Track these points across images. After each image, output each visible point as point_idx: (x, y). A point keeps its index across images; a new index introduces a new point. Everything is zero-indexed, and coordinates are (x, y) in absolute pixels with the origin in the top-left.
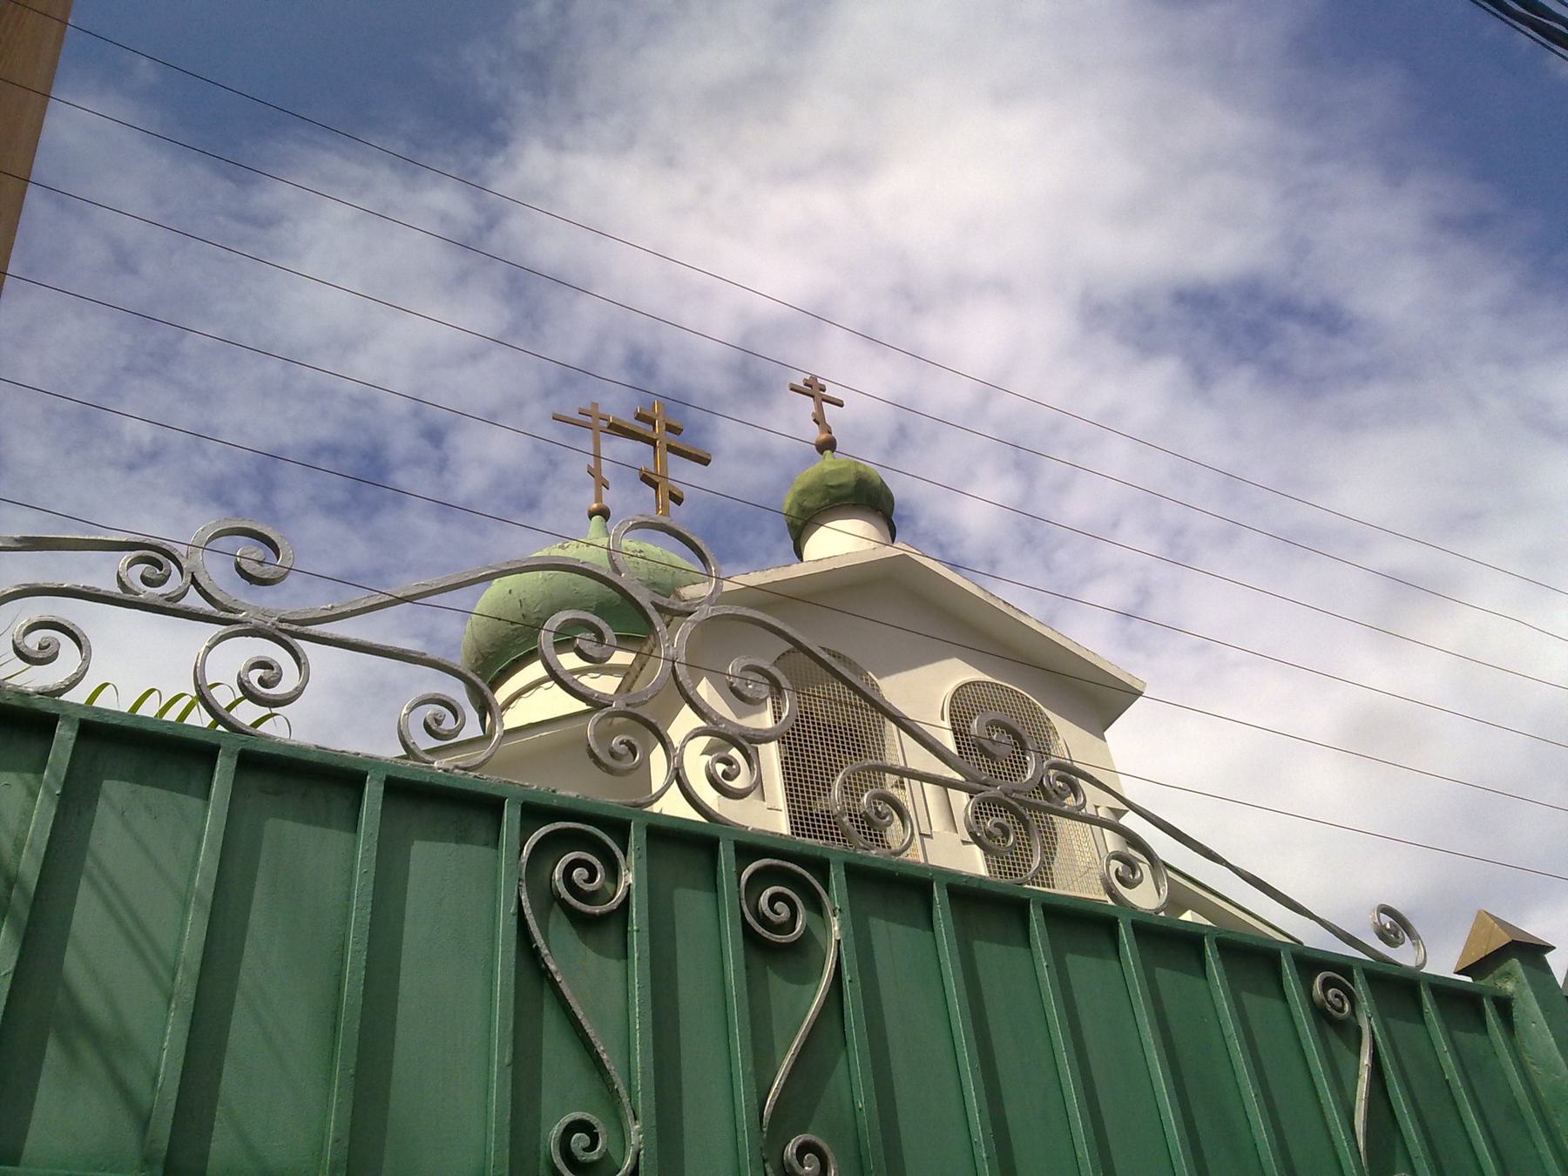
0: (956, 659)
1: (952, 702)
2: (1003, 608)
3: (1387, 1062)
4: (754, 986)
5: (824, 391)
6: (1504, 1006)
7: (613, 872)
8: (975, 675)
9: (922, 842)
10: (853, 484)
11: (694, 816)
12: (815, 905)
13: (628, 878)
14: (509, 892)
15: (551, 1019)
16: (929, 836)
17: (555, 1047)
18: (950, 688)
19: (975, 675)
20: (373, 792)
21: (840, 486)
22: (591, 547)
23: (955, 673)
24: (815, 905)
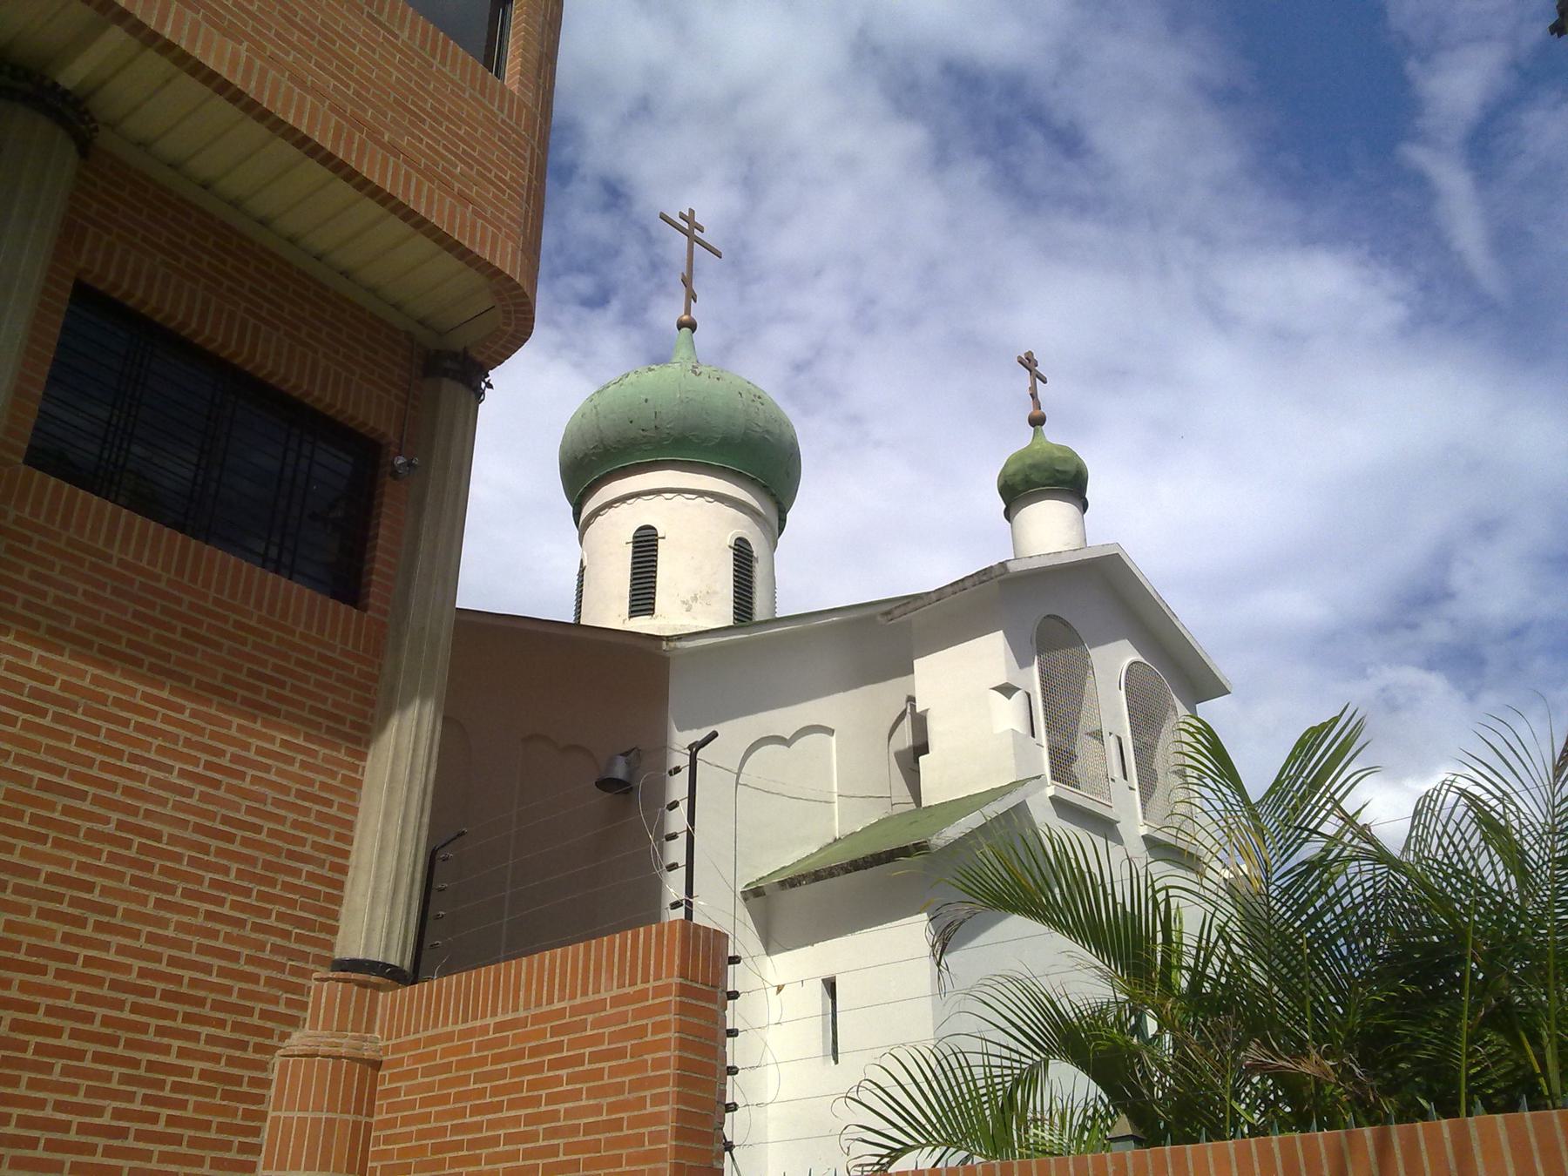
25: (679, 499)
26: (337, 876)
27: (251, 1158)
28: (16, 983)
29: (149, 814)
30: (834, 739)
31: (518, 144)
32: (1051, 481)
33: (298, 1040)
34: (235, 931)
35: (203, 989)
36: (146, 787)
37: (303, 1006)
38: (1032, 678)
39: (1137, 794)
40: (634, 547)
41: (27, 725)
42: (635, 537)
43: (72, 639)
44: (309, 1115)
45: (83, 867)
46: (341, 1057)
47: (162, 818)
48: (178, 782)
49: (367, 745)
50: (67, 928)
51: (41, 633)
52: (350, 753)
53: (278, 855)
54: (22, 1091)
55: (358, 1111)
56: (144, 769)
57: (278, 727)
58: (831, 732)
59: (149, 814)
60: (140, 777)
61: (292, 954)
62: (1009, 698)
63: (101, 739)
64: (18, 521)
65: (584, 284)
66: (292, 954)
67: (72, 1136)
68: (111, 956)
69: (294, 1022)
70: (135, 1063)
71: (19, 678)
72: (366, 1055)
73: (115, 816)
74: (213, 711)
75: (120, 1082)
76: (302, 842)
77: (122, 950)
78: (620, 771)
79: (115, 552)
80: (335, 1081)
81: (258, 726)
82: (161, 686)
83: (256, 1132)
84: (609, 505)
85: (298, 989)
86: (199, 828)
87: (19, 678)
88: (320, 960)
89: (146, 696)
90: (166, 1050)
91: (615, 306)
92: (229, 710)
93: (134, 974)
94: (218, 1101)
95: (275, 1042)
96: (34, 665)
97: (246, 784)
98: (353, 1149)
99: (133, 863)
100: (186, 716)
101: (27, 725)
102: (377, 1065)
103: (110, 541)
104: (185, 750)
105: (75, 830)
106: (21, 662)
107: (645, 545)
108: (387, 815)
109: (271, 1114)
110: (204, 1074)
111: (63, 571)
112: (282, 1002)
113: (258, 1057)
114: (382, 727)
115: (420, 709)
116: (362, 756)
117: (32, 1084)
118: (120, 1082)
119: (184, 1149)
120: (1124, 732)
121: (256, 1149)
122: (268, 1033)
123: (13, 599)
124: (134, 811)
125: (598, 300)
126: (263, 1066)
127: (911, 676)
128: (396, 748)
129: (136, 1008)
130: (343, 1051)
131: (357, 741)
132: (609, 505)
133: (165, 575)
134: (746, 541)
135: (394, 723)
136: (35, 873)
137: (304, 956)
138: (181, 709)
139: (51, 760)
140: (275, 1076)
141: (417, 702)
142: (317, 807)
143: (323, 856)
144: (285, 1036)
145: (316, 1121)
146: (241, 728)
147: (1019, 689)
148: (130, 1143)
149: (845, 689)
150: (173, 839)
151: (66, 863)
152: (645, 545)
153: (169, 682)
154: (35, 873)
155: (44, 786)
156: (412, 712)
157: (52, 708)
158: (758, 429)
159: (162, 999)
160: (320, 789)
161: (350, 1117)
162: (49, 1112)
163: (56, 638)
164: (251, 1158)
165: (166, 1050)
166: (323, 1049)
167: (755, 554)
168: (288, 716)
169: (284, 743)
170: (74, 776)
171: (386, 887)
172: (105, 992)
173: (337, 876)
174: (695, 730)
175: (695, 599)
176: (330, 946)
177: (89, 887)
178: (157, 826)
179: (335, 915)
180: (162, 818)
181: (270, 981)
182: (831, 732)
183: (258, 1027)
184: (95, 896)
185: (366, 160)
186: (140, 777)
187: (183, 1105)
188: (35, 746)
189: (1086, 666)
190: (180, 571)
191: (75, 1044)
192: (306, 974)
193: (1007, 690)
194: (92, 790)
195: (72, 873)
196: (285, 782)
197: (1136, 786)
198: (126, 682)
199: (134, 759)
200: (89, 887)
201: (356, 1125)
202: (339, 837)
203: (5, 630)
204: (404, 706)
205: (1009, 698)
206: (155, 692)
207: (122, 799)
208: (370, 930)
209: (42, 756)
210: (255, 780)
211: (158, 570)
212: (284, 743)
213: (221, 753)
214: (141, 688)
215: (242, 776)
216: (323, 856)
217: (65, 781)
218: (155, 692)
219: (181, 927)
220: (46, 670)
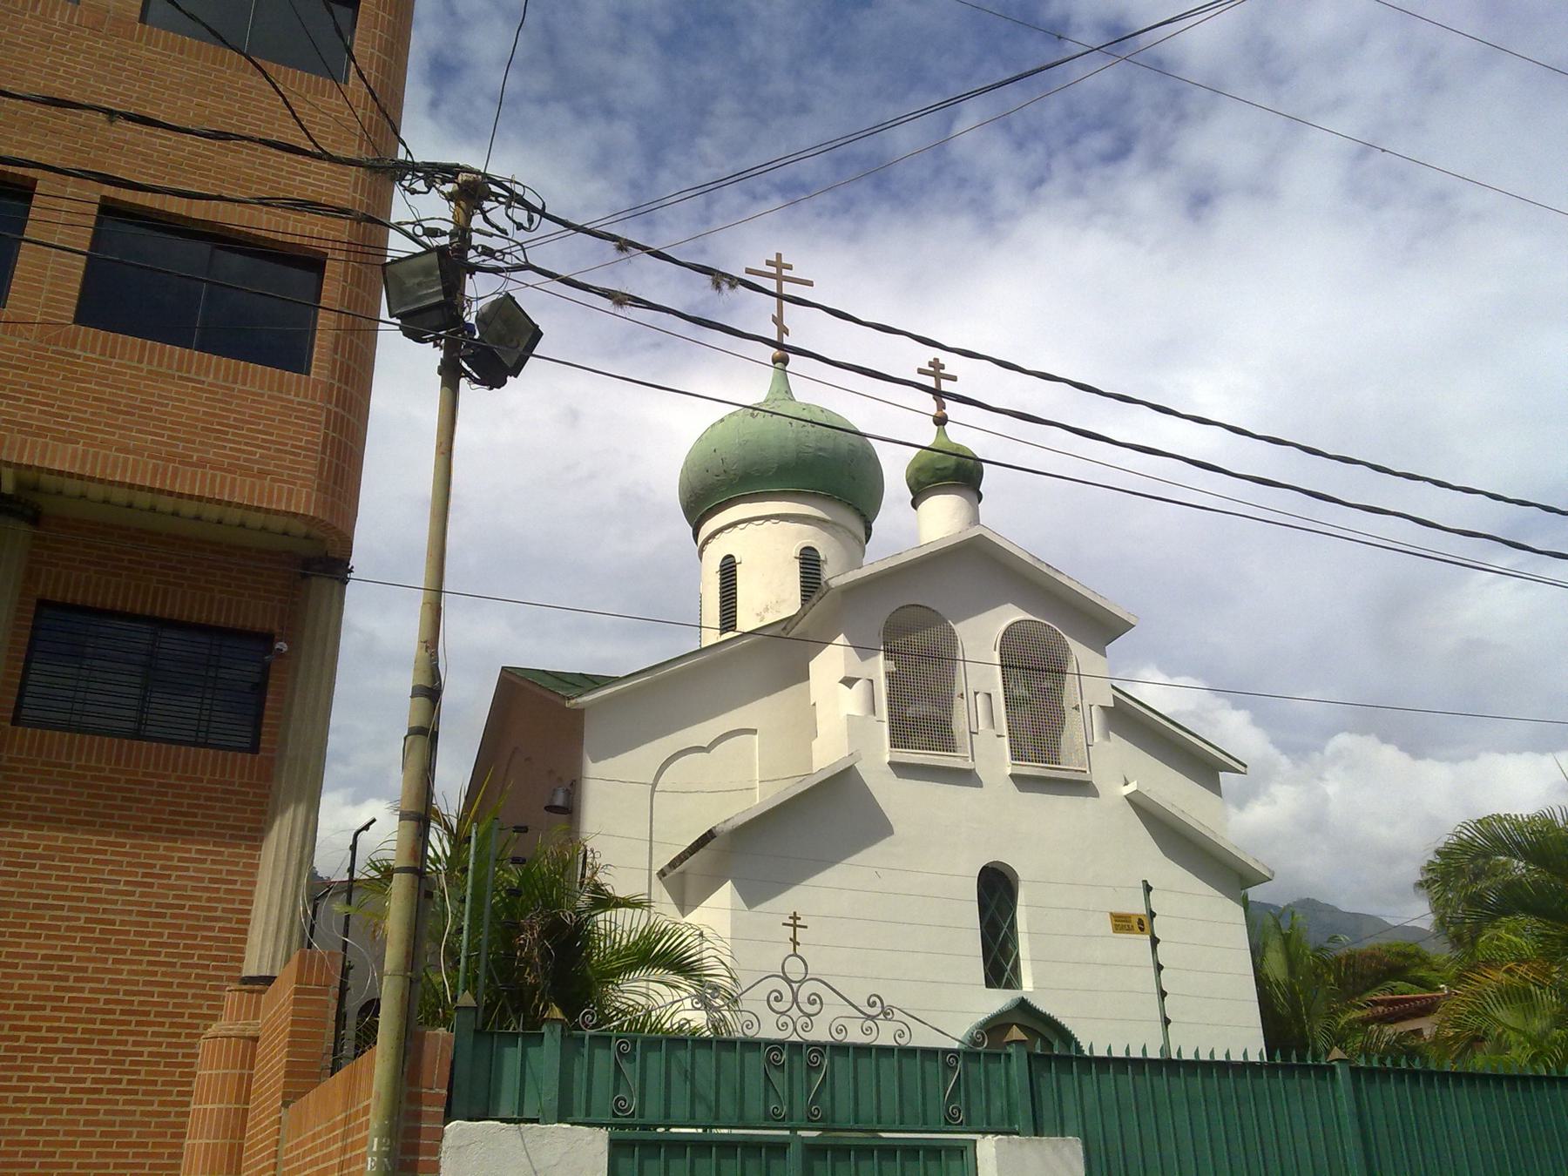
0: (1010, 605)
1: (1002, 640)
2: (1045, 569)
3: (962, 1077)
4: (808, 1075)
5: (943, 368)
6: (1009, 1056)
7: (782, 1055)
8: (1021, 615)
9: (971, 738)
10: (953, 467)
11: (800, 1040)
12: (822, 1056)
13: (784, 1056)
14: (763, 1064)
15: (771, 1088)
16: (977, 733)
17: (772, 1093)
18: (1003, 627)
19: (1021, 615)
20: (738, 1045)
21: (945, 468)
22: (775, 416)
23: (1011, 615)
24: (822, 1056)
25: (751, 526)
26: (242, 926)
27: (186, 1099)
28: (27, 1017)
29: (105, 911)
30: (757, 736)
31: (313, 414)
32: (933, 480)
33: (215, 1028)
34: (170, 970)
35: (148, 1006)
36: (103, 896)
37: (221, 1008)
38: (879, 666)
39: (1006, 740)
40: (721, 575)
41: (24, 875)
42: (721, 566)
43: (48, 819)
44: (214, 1072)
45: (64, 948)
46: (231, 1037)
47: (114, 912)
48: (125, 888)
49: (262, 841)
50: (56, 983)
51: (29, 821)
52: (249, 847)
53: (198, 920)
54: (35, 1073)
55: (242, 1067)
56: (101, 885)
57: (193, 842)
58: (754, 732)
59: (105, 911)
60: (99, 890)
61: (210, 978)
62: (850, 688)
63: (72, 874)
64: (10, 760)
65: (1099, 142)
66: (210, 978)
67: (67, 1095)
68: (86, 995)
69: (214, 1018)
70: (105, 1052)
71: (16, 850)
72: (247, 1034)
73: (83, 916)
74: (146, 842)
75: (95, 1063)
76: (215, 909)
77: (92, 990)
78: (559, 800)
79: (73, 761)
80: (228, 1051)
81: (179, 844)
82: (109, 834)
83: (190, 1084)
84: (721, 530)
85: (217, 998)
86: (140, 913)
87: (16, 850)
88: (231, 979)
89: (99, 843)
90: (125, 1043)
91: (1141, 150)
92: (157, 839)
93: (101, 1003)
94: (161, 1068)
95: (200, 1031)
96: (25, 840)
97: (172, 881)
98: (239, 1090)
99: (97, 940)
100: (127, 849)
101: (24, 875)
102: (255, 1039)
103: (69, 756)
104: (128, 869)
105: (58, 928)
106: (17, 840)
107: (728, 570)
108: (273, 882)
109: (199, 1073)
110: (151, 1054)
111: (40, 782)
112: (205, 1007)
113: (188, 1041)
114: (271, 827)
115: (294, 811)
116: (259, 848)
117: (41, 1069)
118: (95, 1063)
119: (140, 1097)
120: (996, 687)
121: (190, 1094)
122: (197, 1026)
123: (9, 806)
124: (96, 911)
125: (1119, 153)
126: (192, 1046)
127: (806, 683)
128: (278, 840)
129: (103, 1022)
130: (231, 1033)
131: (255, 839)
132: (721, 530)
133: (108, 768)
134: (813, 549)
135: (277, 823)
136: (35, 956)
137: (220, 978)
138: (124, 845)
139: (40, 891)
140: (200, 1051)
141: (291, 810)
142: (224, 886)
143: (231, 916)
144: (206, 1027)
145: (217, 1075)
146: (166, 848)
147: (859, 679)
148: (104, 1096)
149: (769, 694)
150: (123, 923)
151: (54, 947)
152: (728, 570)
153: (114, 831)
154: (35, 956)
155: (37, 906)
156: (289, 814)
157: (38, 862)
158: (810, 450)
159: (120, 1014)
160: (227, 875)
161: (237, 1071)
162: (52, 1083)
163: (39, 821)
164: (186, 1099)
165: (125, 1043)
166: (224, 1033)
167: (822, 558)
168: (201, 833)
169: (198, 851)
170: (55, 898)
171: (272, 928)
172: (83, 1015)
173: (242, 926)
174: (610, 760)
175: (767, 609)
176: (240, 969)
177: (70, 958)
178: (112, 917)
179: (242, 951)
180: (114, 912)
181: (195, 996)
182: (754, 732)
183: (189, 1024)
184: (74, 963)
185: (179, 480)
186: (99, 890)
187: (138, 1072)
188: (30, 886)
189: (952, 638)
190: (118, 761)
191: (66, 1046)
192: (221, 988)
193: (849, 682)
194: (67, 904)
195: (58, 952)
196: (200, 875)
197: (1006, 733)
198: (86, 837)
199: (94, 880)
200: (70, 958)
201: (241, 1076)
202: (242, 902)
203: (6, 825)
204: (283, 812)
205: (850, 688)
206: (106, 839)
207: (87, 905)
208: (261, 958)
209: (35, 891)
210: (179, 877)
211: (103, 765)
212: (198, 851)
213: (154, 866)
214: (96, 838)
215: (169, 877)
216: (231, 916)
217: (50, 901)
218: (106, 839)
219: (131, 972)
220: (33, 842)
